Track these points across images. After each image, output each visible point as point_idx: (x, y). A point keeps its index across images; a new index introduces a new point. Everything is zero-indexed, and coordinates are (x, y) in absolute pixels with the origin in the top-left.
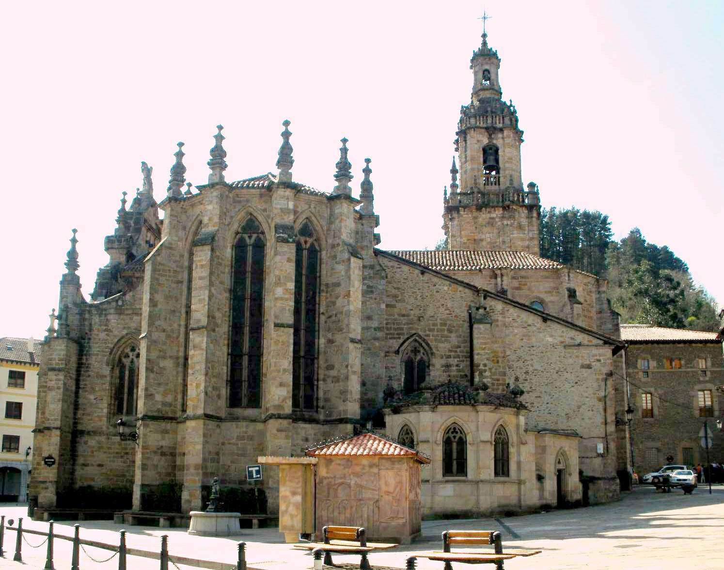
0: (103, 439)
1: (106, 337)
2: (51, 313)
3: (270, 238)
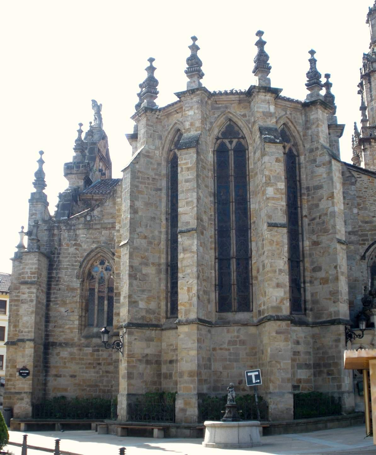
0: (75, 350)
1: (75, 251)
2: (20, 230)
3: (254, 142)
